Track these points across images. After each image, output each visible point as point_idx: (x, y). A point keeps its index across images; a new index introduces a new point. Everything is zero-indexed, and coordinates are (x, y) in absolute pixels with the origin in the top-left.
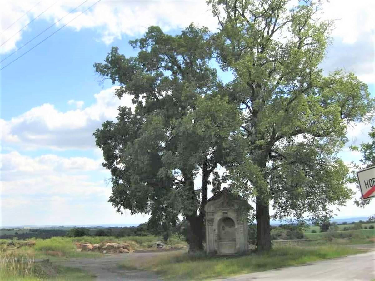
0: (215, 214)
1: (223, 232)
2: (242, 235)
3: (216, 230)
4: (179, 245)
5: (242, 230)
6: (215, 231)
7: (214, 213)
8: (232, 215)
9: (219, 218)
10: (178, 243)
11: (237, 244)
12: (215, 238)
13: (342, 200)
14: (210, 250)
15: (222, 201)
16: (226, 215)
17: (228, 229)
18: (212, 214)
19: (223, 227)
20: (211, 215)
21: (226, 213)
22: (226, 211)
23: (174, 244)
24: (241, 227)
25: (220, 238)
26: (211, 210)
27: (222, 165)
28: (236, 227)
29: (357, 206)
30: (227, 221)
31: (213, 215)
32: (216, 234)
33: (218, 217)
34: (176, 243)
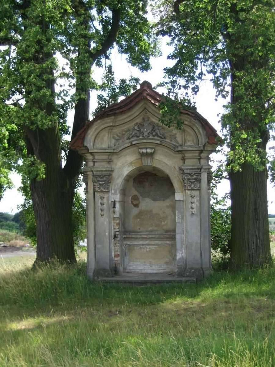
0: (114, 158)
1: (135, 211)
2: (195, 220)
3: (118, 205)
4: (18, 241)
5: (194, 205)
6: (114, 207)
7: (112, 154)
8: (166, 162)
9: (126, 171)
10: (16, 238)
11: (178, 245)
12: (115, 228)
13: (245, 158)
14: (97, 262)
15: (139, 120)
16: (147, 162)
17: (146, 204)
18: (105, 157)
19: (135, 198)
20: (103, 161)
21: (151, 155)
22: (149, 151)
23: (9, 241)
24: (192, 197)
25: (125, 233)
26: (105, 146)
27: (220, 49)
28: (178, 196)
29: (101, 68)
30: (149, 180)
31: (110, 161)
32: (117, 215)
33: (125, 166)
34: (12, 240)
